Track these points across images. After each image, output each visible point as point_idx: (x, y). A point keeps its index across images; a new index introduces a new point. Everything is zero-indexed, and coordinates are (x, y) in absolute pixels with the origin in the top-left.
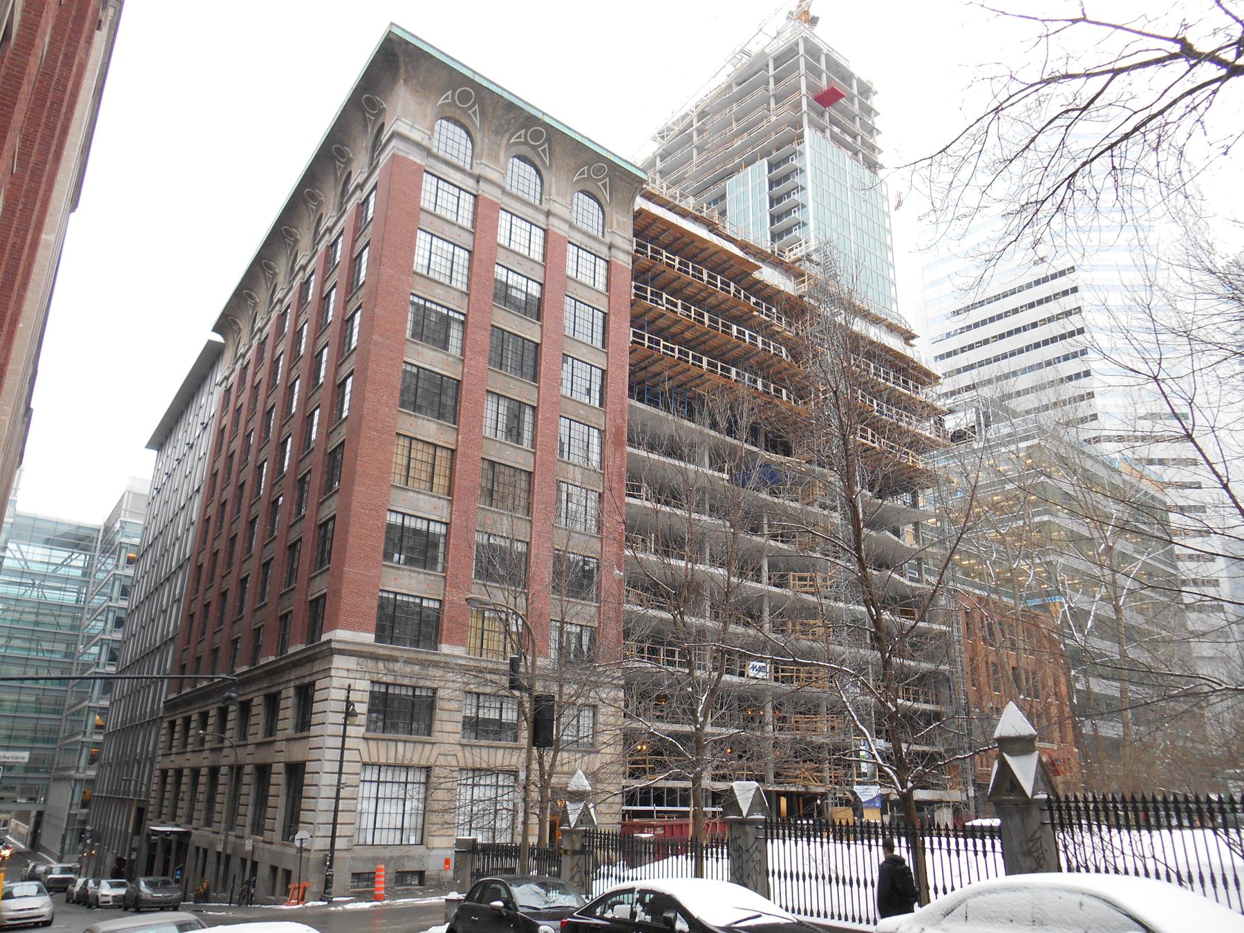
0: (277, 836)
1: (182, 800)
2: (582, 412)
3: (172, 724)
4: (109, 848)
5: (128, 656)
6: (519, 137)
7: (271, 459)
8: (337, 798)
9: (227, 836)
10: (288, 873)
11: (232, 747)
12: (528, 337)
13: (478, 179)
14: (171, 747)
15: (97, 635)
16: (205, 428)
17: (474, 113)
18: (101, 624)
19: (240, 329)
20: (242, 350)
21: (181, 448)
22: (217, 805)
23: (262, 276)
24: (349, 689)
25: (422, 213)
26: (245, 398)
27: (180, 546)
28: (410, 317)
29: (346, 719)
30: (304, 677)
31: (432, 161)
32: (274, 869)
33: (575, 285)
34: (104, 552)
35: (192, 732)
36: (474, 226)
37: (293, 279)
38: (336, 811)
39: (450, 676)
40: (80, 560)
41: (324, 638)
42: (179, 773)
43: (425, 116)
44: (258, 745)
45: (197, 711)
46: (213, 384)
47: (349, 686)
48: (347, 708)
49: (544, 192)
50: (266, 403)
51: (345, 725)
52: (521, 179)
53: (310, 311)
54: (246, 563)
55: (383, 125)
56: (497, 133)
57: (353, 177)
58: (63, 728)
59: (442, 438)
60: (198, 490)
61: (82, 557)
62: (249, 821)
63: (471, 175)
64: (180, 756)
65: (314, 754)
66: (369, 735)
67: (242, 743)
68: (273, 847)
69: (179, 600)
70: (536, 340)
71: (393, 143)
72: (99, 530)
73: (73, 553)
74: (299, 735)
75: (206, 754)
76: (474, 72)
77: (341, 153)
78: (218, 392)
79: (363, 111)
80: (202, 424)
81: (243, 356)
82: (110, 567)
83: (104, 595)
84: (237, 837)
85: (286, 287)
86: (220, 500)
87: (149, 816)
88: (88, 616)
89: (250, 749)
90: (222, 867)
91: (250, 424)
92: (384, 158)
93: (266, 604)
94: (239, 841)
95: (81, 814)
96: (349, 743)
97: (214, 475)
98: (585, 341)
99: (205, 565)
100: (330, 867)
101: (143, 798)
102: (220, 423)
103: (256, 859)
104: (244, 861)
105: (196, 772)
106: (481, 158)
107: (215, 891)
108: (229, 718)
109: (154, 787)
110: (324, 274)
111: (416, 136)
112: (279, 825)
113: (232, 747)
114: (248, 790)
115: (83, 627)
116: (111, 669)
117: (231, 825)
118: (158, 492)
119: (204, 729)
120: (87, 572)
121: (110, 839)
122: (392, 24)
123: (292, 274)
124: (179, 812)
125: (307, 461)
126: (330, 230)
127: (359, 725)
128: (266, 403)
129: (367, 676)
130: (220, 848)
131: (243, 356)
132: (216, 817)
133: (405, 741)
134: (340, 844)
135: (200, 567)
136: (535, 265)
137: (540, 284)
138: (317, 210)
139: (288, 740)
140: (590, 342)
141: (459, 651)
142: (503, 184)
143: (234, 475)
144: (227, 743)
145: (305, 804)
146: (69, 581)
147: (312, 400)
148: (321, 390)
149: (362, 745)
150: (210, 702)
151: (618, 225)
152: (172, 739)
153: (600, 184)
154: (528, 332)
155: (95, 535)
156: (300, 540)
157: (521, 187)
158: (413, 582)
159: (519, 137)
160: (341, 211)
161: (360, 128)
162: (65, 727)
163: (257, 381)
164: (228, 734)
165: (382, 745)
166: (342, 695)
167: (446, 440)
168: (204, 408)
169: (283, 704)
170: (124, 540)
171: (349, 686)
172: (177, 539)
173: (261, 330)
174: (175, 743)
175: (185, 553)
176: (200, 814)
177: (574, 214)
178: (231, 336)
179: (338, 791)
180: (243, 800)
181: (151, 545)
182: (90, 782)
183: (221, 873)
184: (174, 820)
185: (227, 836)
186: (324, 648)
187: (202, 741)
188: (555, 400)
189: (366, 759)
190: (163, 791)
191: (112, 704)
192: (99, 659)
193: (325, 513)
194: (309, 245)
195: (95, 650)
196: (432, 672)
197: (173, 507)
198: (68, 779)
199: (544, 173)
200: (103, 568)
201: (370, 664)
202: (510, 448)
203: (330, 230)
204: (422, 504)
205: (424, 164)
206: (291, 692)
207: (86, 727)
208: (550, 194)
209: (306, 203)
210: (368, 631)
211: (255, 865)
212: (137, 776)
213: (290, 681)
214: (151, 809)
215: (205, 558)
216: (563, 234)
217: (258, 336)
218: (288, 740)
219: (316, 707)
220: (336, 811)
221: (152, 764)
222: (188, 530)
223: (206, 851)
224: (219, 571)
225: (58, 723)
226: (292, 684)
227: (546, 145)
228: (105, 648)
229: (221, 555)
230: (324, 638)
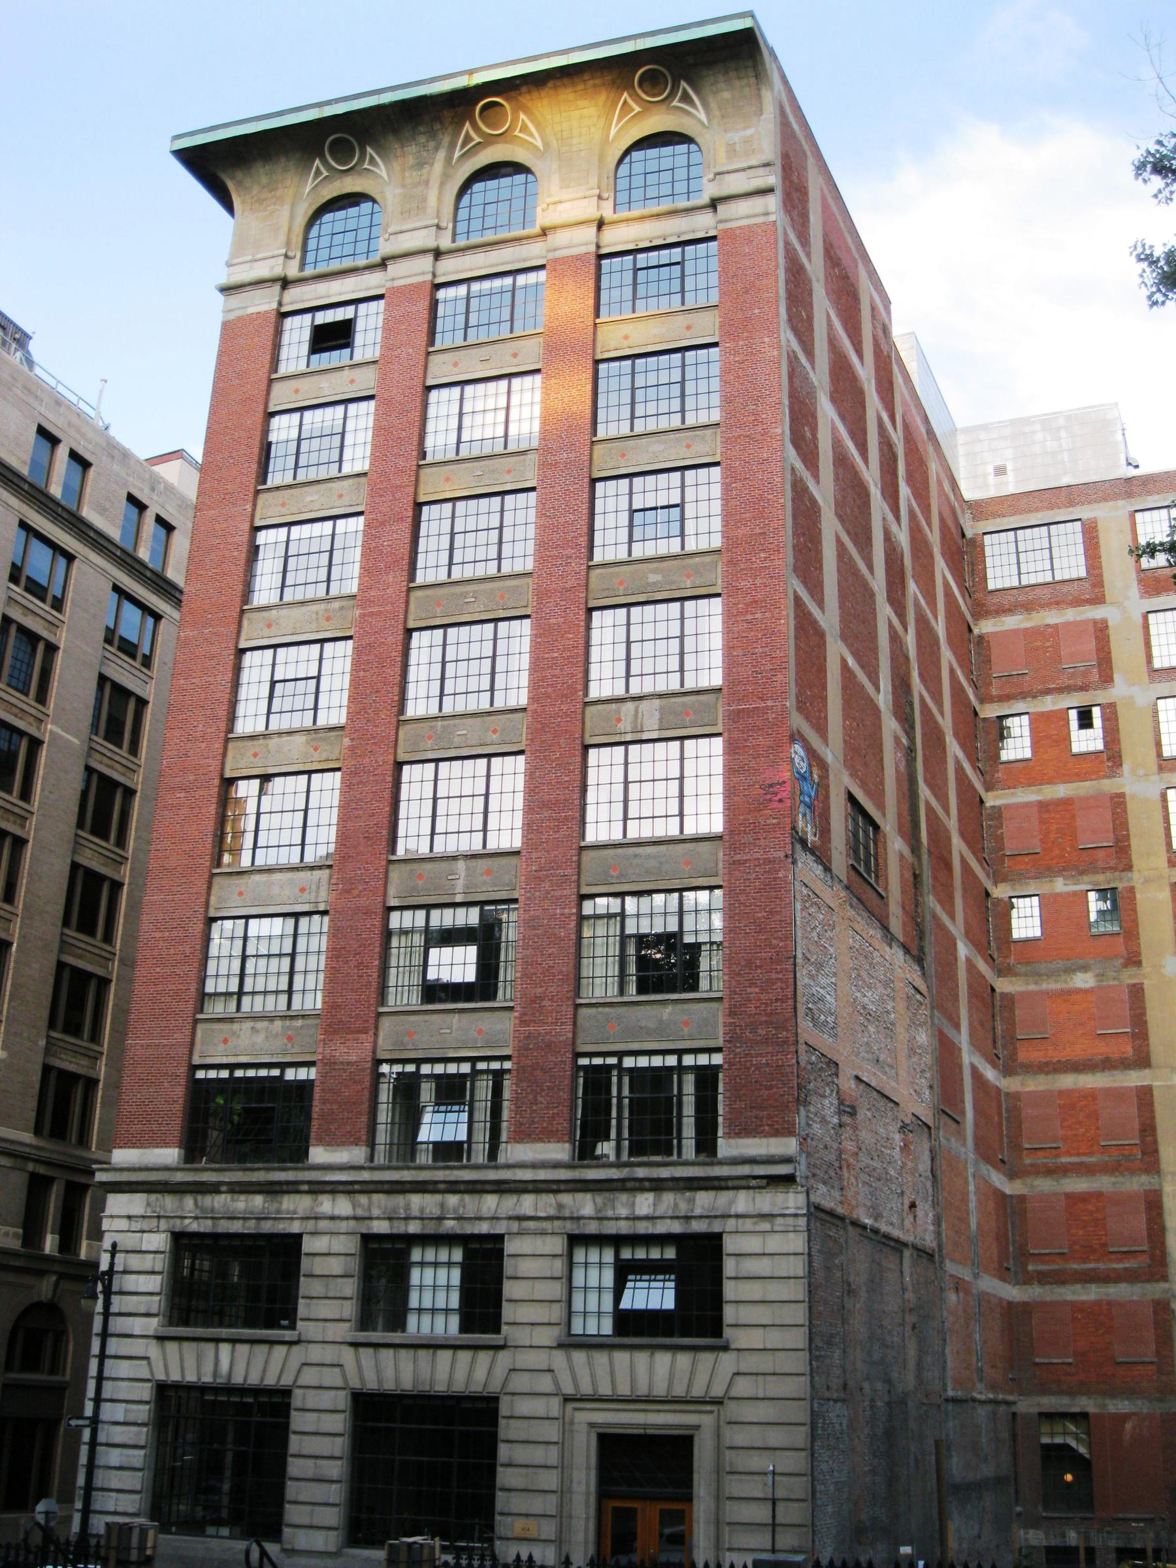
2: (653, 578)
6: (468, 139)
13: (383, 264)
39: (326, 1205)
59: (316, 756)
63: (370, 268)
66: (363, 1336)
129: (163, 1224)
133: (234, 1341)
141: (342, 1156)
149: (153, 1350)
154: (508, 478)
158: (259, 1039)
165: (189, 1348)
167: (324, 756)
189: (568, 1389)
196: (289, 1203)
201: (169, 1202)
204: (276, 890)
210: (166, 1145)
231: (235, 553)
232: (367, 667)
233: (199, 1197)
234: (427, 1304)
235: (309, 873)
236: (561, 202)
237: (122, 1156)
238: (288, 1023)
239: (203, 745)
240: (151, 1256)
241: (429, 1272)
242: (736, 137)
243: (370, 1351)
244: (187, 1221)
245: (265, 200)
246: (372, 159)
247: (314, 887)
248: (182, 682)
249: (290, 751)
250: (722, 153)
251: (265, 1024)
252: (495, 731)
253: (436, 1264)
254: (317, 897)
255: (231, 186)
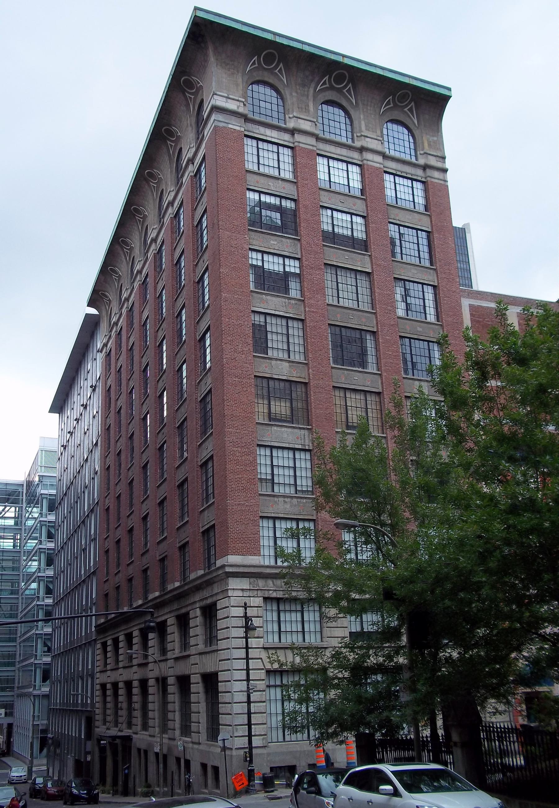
0: (203, 737)
1: (121, 709)
2: (419, 329)
3: (104, 645)
4: (68, 751)
5: (61, 589)
6: (324, 83)
7: (152, 411)
8: (249, 702)
9: (162, 738)
10: (216, 769)
11: (155, 662)
12: (359, 269)
14: (106, 664)
15: (34, 573)
16: (94, 390)
17: (280, 71)
18: (35, 563)
19: (110, 300)
20: (114, 320)
21: (78, 409)
22: (150, 712)
23: (121, 252)
24: (245, 606)
25: (248, 175)
26: (123, 359)
27: (89, 493)
28: (251, 278)
29: (246, 632)
30: (206, 598)
31: (250, 126)
32: (204, 766)
33: (397, 211)
34: (29, 502)
35: (121, 651)
36: (295, 177)
37: (148, 252)
38: (249, 714)
40: (11, 512)
41: (219, 563)
42: (115, 685)
43: (237, 85)
44: (177, 659)
45: (122, 633)
46: (95, 351)
47: (245, 604)
48: (247, 623)
49: (355, 130)
50: (140, 363)
51: (247, 638)
52: (332, 123)
53: (165, 279)
54: (145, 503)
55: (202, 101)
56: (304, 85)
57: (184, 152)
58: (18, 653)
60: (96, 444)
61: (13, 509)
62: (177, 725)
63: (286, 130)
64: (114, 672)
65: (224, 665)
67: (164, 658)
68: (201, 747)
69: (95, 539)
70: (367, 270)
71: (213, 117)
72: (23, 485)
73: (6, 506)
74: (209, 649)
75: (135, 669)
76: (344, 56)
77: (170, 133)
78: (100, 357)
79: (184, 92)
80: (91, 387)
81: (116, 324)
82: (36, 515)
83: (35, 538)
84: (170, 739)
85: (142, 259)
86: (115, 451)
87: (97, 723)
88: (25, 558)
89: (170, 663)
90: (161, 766)
91: (130, 383)
92: (208, 131)
93: (166, 538)
94: (172, 742)
95: (42, 724)
96: (252, 653)
97: (107, 429)
98: (413, 262)
99: (111, 508)
100: (251, 761)
101: (89, 709)
102: (106, 384)
103: (188, 757)
104: (178, 760)
105: (115, 685)
106: (293, 112)
107: (158, 786)
108: (150, 638)
109: (98, 699)
110: (172, 243)
111: (232, 106)
112: (203, 727)
113: (155, 662)
114: (174, 697)
115: (22, 567)
116: (49, 601)
117: (164, 729)
118: (65, 448)
119: (130, 647)
120: (18, 519)
121: (68, 744)
122: (196, 9)
123: (146, 247)
124: (120, 720)
125: (183, 410)
126: (171, 203)
127: (258, 637)
128: (140, 363)
129: (260, 593)
130: (157, 750)
131: (116, 324)
132: (151, 723)
134: (256, 741)
135: (108, 509)
136: (357, 200)
137: (363, 217)
138: (158, 187)
139: (200, 654)
140: (418, 263)
142: (317, 132)
143: (123, 429)
144: (150, 659)
145: (222, 708)
146: (6, 531)
147: (178, 355)
148: (185, 346)
150: (133, 624)
151: (429, 145)
152: (106, 658)
153: (406, 109)
155: (20, 490)
156: (186, 479)
157: (332, 130)
158: (288, 506)
159: (324, 83)
160: (179, 185)
161: (183, 108)
162: (19, 651)
163: (130, 344)
164: (151, 651)
166: (240, 612)
167: (298, 375)
168: (91, 372)
169: (192, 623)
170: (43, 492)
171: (245, 604)
172: (86, 487)
173: (127, 299)
174: (109, 661)
175: (94, 499)
176: (138, 721)
177: (386, 144)
178: (103, 308)
179: (249, 697)
180: (170, 707)
181: (65, 494)
182: (46, 696)
183: (161, 770)
184: (116, 726)
185: (162, 738)
186: (220, 572)
187: (131, 658)
188: (392, 323)
190: (105, 702)
191: (54, 630)
192: (39, 593)
193: (205, 454)
194: (156, 219)
195: (34, 585)
197: (78, 460)
198: (28, 695)
199: (352, 112)
200: (30, 516)
201: (261, 583)
202: (357, 374)
203: (171, 203)
204: (285, 436)
205: (243, 129)
206: (198, 612)
207: (36, 651)
208: (361, 131)
209: (148, 182)
211: (188, 763)
212: (82, 691)
213: (195, 603)
214: (97, 717)
215: (110, 502)
216: (378, 165)
217: (126, 305)
218: (200, 654)
219: (221, 624)
220: (249, 714)
221: (93, 678)
222: (93, 479)
223: (146, 752)
224: (125, 511)
225: (14, 649)
226: (198, 605)
227: (350, 85)
228: (42, 583)
229: (123, 497)
230: (219, 563)
231: (243, 259)
232: (315, 337)
233: (274, 581)
234: (289, 629)
235: (299, 430)
236: (367, 137)
237: (233, 559)
238: (299, 500)
239: (243, 356)
240: (256, 608)
241: (288, 615)
242: (431, 139)
243: (282, 651)
244: (271, 592)
245: (228, 64)
246: (280, 71)
247: (302, 437)
248: (227, 320)
249: (282, 368)
250: (426, 145)
251: (289, 500)
252: (368, 381)
253: (291, 611)
254: (304, 442)
255: (212, 58)
